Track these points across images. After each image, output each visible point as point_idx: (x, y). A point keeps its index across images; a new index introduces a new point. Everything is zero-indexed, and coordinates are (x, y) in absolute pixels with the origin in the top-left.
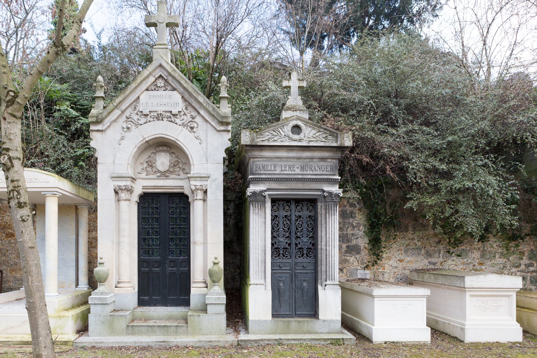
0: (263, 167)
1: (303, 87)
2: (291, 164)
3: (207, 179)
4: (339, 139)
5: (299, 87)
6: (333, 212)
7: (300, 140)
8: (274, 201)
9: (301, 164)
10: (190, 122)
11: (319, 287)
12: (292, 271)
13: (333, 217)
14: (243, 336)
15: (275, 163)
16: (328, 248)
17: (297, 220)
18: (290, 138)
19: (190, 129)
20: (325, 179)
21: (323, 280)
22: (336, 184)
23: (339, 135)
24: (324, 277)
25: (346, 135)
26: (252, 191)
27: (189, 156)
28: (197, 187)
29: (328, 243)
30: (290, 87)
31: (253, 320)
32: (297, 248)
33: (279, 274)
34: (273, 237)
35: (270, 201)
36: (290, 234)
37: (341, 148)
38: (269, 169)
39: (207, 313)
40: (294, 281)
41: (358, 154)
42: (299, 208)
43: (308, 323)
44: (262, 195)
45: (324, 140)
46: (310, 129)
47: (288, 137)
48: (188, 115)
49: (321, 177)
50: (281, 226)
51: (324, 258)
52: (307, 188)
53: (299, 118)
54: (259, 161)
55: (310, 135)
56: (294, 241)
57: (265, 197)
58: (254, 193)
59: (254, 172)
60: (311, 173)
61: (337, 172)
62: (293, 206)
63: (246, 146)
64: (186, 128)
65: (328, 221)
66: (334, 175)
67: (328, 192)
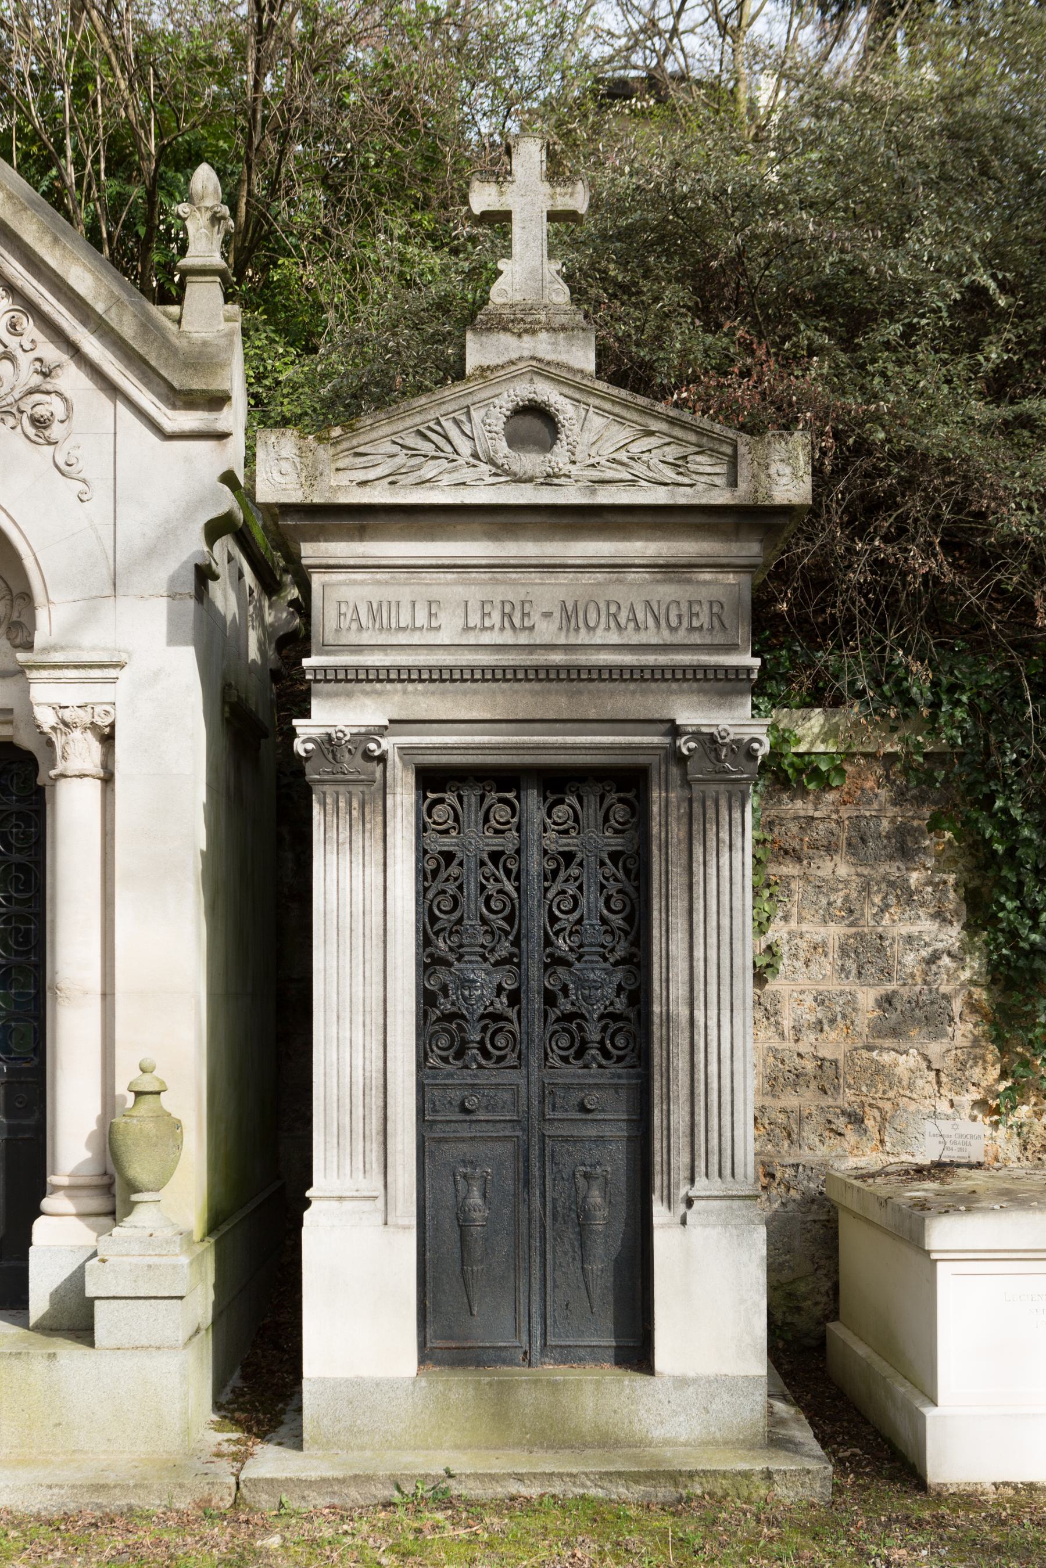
0: (374, 615)
1: (574, 213)
2: (512, 594)
3: (111, 673)
4: (744, 470)
5: (553, 216)
6: (724, 835)
7: (550, 479)
8: (432, 779)
9: (561, 594)
10: (31, 392)
11: (659, 1210)
12: (527, 1130)
13: (725, 860)
14: (270, 1461)
15: (435, 592)
16: (699, 1015)
17: (555, 873)
18: (500, 470)
19: (31, 431)
20: (684, 669)
21: (680, 1173)
22: (741, 693)
23: (742, 449)
24: (681, 1159)
25: (779, 449)
26: (315, 732)
27: (29, 563)
28: (67, 715)
29: (699, 986)
30: (506, 216)
31: (323, 1381)
32: (554, 1014)
33: (464, 1148)
34: (429, 962)
35: (411, 779)
36: (516, 943)
37: (755, 518)
38: (405, 620)
39: (91, 1344)
40: (536, 1181)
41: (887, 539)
42: (561, 812)
43: (599, 1393)
44: (367, 756)
45: (670, 474)
46: (597, 422)
47: (491, 462)
48: (24, 360)
49: (663, 659)
50: (472, 903)
51: (681, 1063)
52: (592, 714)
53: (542, 369)
54: (354, 583)
55: (607, 450)
56: (536, 978)
57: (382, 759)
58: (329, 745)
59: (330, 638)
60: (614, 638)
61: (743, 633)
62: (532, 801)
63: (287, 509)
64: (11, 421)
65: (698, 877)
66: (731, 648)
67: (696, 735)
